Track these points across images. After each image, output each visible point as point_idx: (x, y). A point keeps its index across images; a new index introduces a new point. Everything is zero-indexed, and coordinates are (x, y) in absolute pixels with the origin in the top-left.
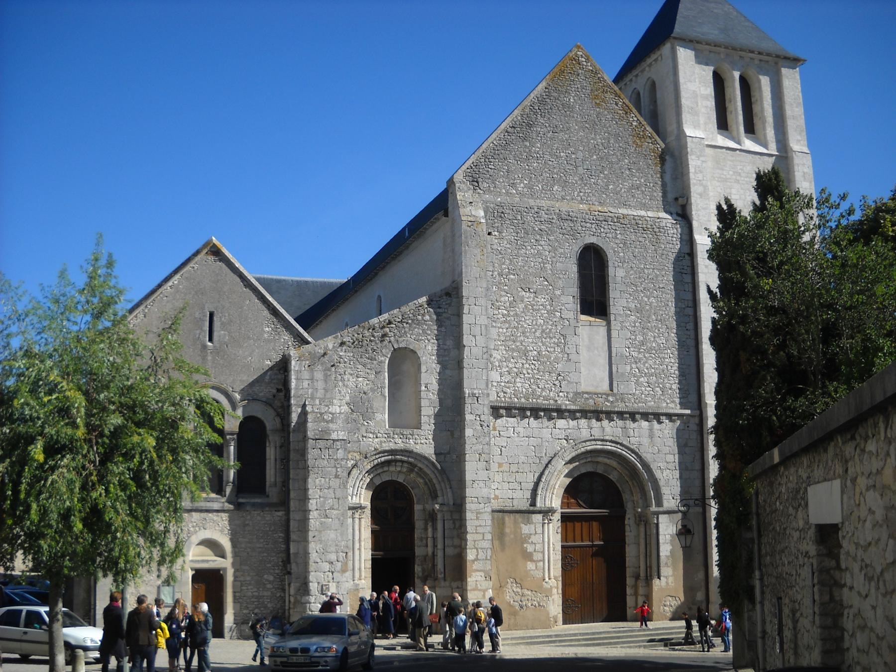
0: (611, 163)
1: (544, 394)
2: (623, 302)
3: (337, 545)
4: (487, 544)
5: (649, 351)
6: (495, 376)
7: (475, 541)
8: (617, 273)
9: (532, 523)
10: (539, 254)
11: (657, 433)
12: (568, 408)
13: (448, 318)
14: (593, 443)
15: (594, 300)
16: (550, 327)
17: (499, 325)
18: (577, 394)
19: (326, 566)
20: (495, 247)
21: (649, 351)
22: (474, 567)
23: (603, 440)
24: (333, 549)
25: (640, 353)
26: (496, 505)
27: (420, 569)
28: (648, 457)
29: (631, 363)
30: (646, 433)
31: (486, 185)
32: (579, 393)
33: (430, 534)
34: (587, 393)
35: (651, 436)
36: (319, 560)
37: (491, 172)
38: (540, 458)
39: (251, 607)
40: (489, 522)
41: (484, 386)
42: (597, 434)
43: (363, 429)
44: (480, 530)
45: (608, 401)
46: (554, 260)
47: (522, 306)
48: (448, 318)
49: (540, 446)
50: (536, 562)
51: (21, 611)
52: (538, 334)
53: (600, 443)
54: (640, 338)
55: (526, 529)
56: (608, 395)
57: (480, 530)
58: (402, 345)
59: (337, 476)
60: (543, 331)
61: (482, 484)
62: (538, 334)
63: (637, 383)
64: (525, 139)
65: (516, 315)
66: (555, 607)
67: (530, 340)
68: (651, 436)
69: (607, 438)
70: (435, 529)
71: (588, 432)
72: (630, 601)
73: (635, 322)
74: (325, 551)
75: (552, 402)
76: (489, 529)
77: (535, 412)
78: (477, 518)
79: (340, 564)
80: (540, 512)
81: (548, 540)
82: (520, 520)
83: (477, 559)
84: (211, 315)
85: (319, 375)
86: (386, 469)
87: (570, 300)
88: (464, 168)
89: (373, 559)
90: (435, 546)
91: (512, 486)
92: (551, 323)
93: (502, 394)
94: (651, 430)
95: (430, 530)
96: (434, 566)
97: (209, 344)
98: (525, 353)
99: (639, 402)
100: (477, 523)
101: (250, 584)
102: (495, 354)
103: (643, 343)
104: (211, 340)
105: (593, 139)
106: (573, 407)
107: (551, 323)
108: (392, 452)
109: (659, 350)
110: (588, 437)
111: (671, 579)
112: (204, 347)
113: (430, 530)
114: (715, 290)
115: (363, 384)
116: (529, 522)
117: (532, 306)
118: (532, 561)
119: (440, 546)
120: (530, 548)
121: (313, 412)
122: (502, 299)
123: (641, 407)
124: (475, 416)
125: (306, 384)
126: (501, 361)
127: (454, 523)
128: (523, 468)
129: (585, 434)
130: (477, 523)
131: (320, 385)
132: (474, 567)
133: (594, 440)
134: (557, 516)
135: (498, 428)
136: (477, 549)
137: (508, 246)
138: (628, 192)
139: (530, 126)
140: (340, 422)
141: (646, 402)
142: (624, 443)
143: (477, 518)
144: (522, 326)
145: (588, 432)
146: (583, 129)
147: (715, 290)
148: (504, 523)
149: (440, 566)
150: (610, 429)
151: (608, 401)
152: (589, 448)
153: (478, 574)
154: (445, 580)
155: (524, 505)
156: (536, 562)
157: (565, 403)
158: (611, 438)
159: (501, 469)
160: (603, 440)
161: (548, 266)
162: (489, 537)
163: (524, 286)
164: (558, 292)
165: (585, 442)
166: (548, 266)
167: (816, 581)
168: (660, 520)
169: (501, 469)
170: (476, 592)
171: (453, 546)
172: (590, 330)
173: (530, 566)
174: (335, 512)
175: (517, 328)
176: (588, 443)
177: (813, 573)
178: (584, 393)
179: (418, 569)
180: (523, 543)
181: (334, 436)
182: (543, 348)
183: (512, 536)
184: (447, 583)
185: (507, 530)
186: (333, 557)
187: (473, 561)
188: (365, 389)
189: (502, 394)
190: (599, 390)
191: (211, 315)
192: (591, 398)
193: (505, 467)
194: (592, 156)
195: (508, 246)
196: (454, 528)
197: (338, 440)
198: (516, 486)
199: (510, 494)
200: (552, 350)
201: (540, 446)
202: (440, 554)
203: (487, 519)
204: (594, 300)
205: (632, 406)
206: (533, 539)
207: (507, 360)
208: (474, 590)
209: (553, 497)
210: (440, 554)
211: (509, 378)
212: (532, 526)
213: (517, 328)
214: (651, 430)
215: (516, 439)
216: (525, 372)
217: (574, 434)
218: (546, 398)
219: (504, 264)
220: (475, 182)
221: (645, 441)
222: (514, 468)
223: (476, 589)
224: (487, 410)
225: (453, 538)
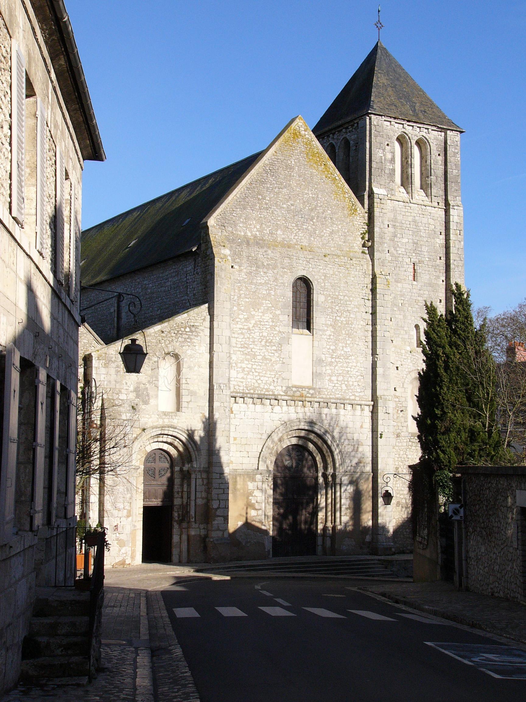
3: (124, 498)
7: (218, 494)
15: (304, 312)
16: (271, 338)
17: (236, 336)
18: (288, 387)
27: (176, 515)
31: (230, 229)
32: (289, 387)
33: (185, 489)
37: (234, 218)
47: (253, 322)
52: (263, 343)
62: (263, 343)
70: (189, 485)
79: (126, 511)
82: (248, 479)
83: (219, 508)
90: (189, 498)
95: (185, 486)
96: (188, 512)
99: (331, 394)
110: (197, 496)
113: (185, 486)
117: (261, 322)
119: (193, 498)
127: (203, 481)
135: (234, 412)
138: (329, 236)
149: (192, 513)
154: (196, 523)
167: (520, 530)
170: (218, 532)
171: (201, 498)
172: (300, 339)
177: (518, 527)
183: (242, 491)
184: (197, 525)
185: (238, 487)
192: (298, 391)
196: (203, 485)
200: (273, 355)
202: (193, 503)
204: (304, 312)
210: (193, 503)
218: (267, 390)
219: (241, 290)
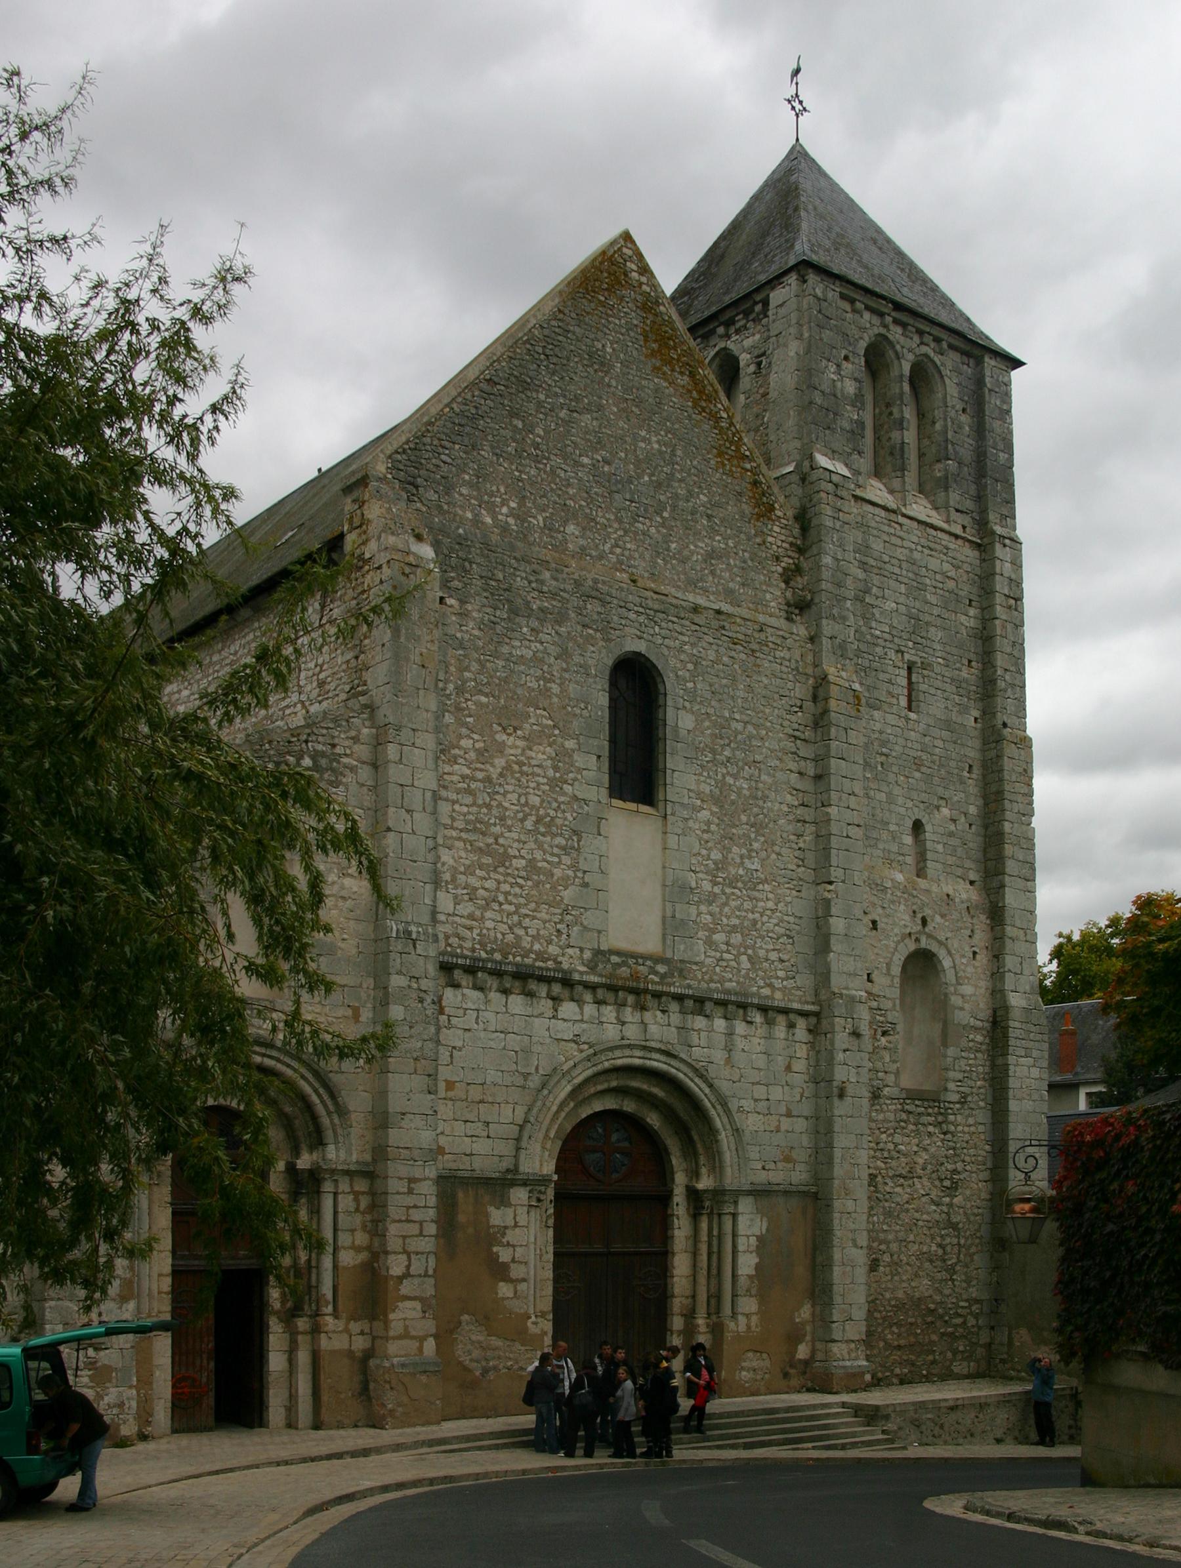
1: (537, 947)
4: (427, 1244)
5: (732, 882)
8: (680, 719)
9: (509, 1205)
11: (740, 1043)
12: (585, 978)
14: (627, 1052)
15: (637, 772)
16: (552, 813)
18: (598, 952)
21: (732, 882)
23: (644, 1048)
25: (715, 884)
26: (447, 1162)
28: (724, 1087)
29: (699, 902)
30: (720, 1040)
34: (618, 953)
35: (729, 1049)
40: (432, 1201)
41: (426, 919)
42: (632, 1033)
44: (416, 1215)
45: (656, 973)
46: (567, 675)
47: (500, 762)
49: (527, 1051)
50: (515, 1282)
52: (529, 824)
53: (638, 1053)
54: (716, 855)
55: (497, 1216)
57: (416, 1215)
60: (538, 821)
62: (529, 824)
65: (488, 780)
67: (515, 836)
68: (729, 1049)
69: (653, 1044)
71: (611, 1028)
73: (708, 823)
75: (550, 964)
76: (432, 1213)
78: (410, 1191)
80: (525, 1183)
83: (407, 1275)
87: (591, 768)
91: (471, 1129)
92: (555, 805)
94: (730, 1034)
98: (504, 859)
99: (712, 981)
100: (410, 1200)
103: (720, 866)
105: (644, 440)
106: (594, 979)
107: (555, 805)
111: (754, 1319)
116: (504, 1202)
117: (521, 764)
118: (507, 1279)
120: (504, 1255)
122: (463, 743)
127: (356, 1200)
128: (493, 1095)
129: (611, 1033)
130: (410, 1200)
133: (629, 1046)
135: (447, 1010)
136: (409, 1254)
137: (476, 632)
139: (525, 386)
141: (722, 981)
142: (683, 1056)
143: (410, 1191)
144: (500, 805)
145: (611, 1028)
150: (660, 1026)
151: (656, 973)
152: (619, 1062)
153: (409, 1304)
156: (515, 1282)
157: (574, 962)
158: (658, 1046)
159: (450, 1094)
160: (644, 1048)
161: (555, 688)
162: (432, 1229)
163: (505, 722)
165: (611, 1049)
166: (555, 688)
168: (741, 1208)
169: (450, 1094)
173: (504, 1290)
175: (488, 806)
176: (618, 1053)
178: (612, 952)
180: (492, 1245)
182: (538, 855)
183: (471, 1230)
185: (462, 1218)
187: (400, 1279)
190: (641, 949)
194: (639, 477)
195: (476, 632)
196: (357, 1210)
198: (478, 1129)
199: (466, 1145)
201: (527, 1051)
203: (428, 1192)
204: (637, 772)
205: (695, 984)
206: (510, 1236)
207: (469, 871)
208: (400, 1337)
209: (541, 1160)
212: (510, 1211)
213: (488, 806)
214: (730, 1034)
215: (482, 1034)
216: (501, 898)
217: (591, 1033)
218: (540, 956)
219: (467, 669)
221: (719, 1056)
223: (406, 1335)
225: (353, 1231)
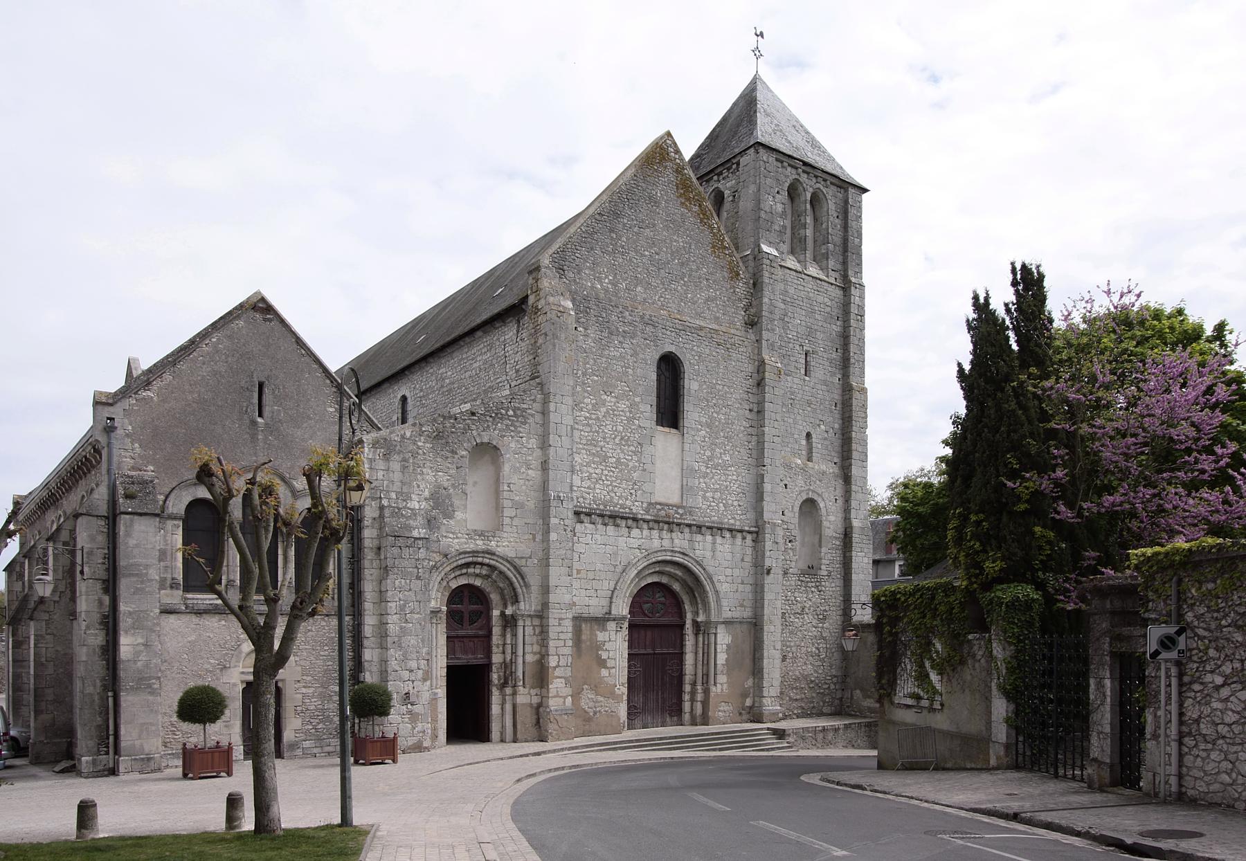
0: (691, 270)
2: (695, 416)
4: (567, 651)
6: (577, 481)
8: (691, 385)
10: (622, 357)
13: (532, 415)
15: (670, 412)
19: (406, 674)
20: (580, 344)
22: (556, 674)
24: (414, 656)
26: (577, 610)
28: (710, 569)
36: (397, 668)
38: (615, 566)
39: (315, 722)
40: (570, 629)
41: (568, 490)
42: (666, 543)
43: (443, 528)
44: (562, 636)
48: (532, 415)
49: (616, 554)
51: (471, 603)
52: (617, 441)
54: (708, 453)
55: (601, 636)
56: (678, 507)
57: (562, 636)
58: (486, 440)
59: (418, 578)
61: (564, 590)
62: (617, 441)
63: (704, 497)
64: (611, 231)
65: (598, 418)
66: (622, 711)
70: (515, 635)
72: (687, 706)
74: (405, 658)
76: (570, 635)
77: (613, 518)
81: (616, 646)
83: (558, 666)
84: (261, 386)
85: (396, 465)
86: (464, 571)
87: (648, 410)
88: (550, 251)
89: (448, 667)
90: (514, 653)
93: (581, 500)
97: (260, 420)
98: (605, 458)
100: (559, 629)
101: (313, 697)
102: (577, 458)
103: (710, 459)
104: (260, 415)
108: (474, 553)
109: (725, 467)
111: (725, 686)
112: (254, 423)
113: (508, 636)
114: (967, 367)
115: (443, 479)
116: (604, 629)
118: (606, 667)
119: (520, 652)
120: (604, 656)
121: (390, 506)
123: (706, 521)
124: (561, 515)
125: (380, 474)
126: (581, 465)
129: (656, 544)
130: (559, 629)
131: (397, 476)
132: (556, 674)
134: (626, 625)
140: (420, 518)
146: (667, 228)
147: (967, 367)
148: (580, 630)
150: (680, 541)
155: (598, 612)
162: (570, 643)
164: (637, 399)
173: (604, 672)
174: (417, 616)
179: (495, 677)
181: (415, 534)
182: (622, 456)
185: (584, 637)
186: (413, 664)
188: (446, 484)
189: (581, 500)
190: (670, 502)
191: (261, 386)
193: (583, 575)
197: (419, 539)
198: (592, 592)
201: (616, 554)
204: (670, 412)
205: (698, 518)
206: (607, 646)
207: (588, 465)
209: (622, 608)
210: (520, 660)
211: (589, 483)
217: (646, 544)
218: (622, 506)
220: (561, 270)
221: (708, 554)
222: (591, 575)
223: (557, 696)
224: (571, 515)
